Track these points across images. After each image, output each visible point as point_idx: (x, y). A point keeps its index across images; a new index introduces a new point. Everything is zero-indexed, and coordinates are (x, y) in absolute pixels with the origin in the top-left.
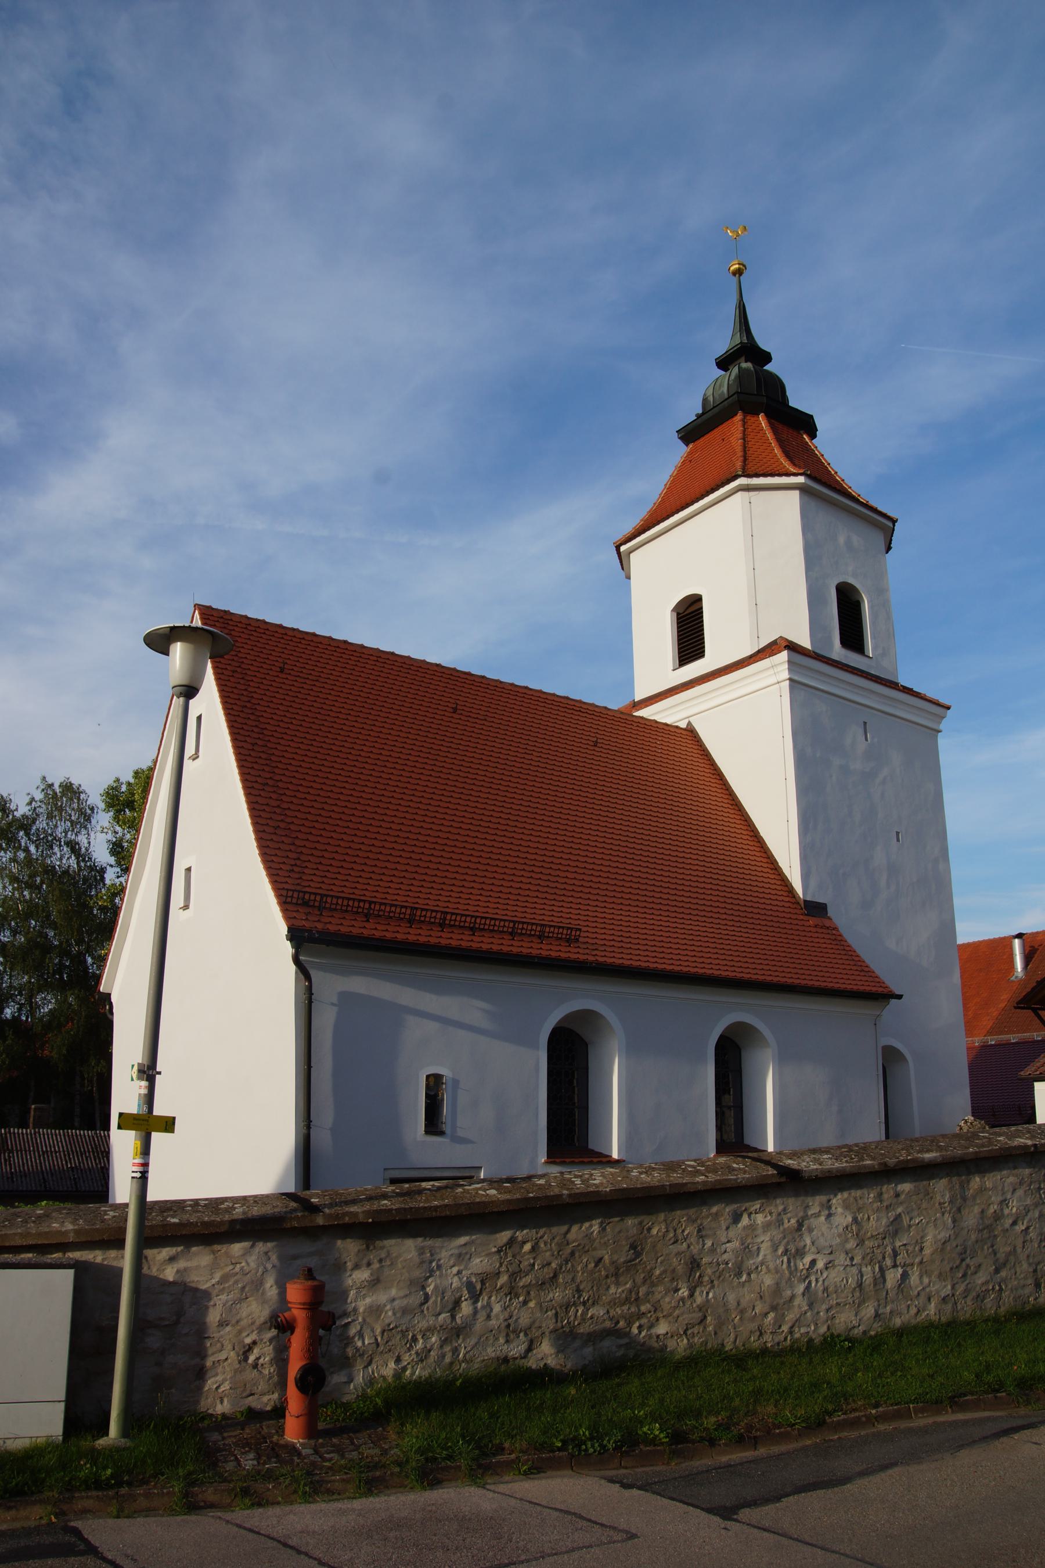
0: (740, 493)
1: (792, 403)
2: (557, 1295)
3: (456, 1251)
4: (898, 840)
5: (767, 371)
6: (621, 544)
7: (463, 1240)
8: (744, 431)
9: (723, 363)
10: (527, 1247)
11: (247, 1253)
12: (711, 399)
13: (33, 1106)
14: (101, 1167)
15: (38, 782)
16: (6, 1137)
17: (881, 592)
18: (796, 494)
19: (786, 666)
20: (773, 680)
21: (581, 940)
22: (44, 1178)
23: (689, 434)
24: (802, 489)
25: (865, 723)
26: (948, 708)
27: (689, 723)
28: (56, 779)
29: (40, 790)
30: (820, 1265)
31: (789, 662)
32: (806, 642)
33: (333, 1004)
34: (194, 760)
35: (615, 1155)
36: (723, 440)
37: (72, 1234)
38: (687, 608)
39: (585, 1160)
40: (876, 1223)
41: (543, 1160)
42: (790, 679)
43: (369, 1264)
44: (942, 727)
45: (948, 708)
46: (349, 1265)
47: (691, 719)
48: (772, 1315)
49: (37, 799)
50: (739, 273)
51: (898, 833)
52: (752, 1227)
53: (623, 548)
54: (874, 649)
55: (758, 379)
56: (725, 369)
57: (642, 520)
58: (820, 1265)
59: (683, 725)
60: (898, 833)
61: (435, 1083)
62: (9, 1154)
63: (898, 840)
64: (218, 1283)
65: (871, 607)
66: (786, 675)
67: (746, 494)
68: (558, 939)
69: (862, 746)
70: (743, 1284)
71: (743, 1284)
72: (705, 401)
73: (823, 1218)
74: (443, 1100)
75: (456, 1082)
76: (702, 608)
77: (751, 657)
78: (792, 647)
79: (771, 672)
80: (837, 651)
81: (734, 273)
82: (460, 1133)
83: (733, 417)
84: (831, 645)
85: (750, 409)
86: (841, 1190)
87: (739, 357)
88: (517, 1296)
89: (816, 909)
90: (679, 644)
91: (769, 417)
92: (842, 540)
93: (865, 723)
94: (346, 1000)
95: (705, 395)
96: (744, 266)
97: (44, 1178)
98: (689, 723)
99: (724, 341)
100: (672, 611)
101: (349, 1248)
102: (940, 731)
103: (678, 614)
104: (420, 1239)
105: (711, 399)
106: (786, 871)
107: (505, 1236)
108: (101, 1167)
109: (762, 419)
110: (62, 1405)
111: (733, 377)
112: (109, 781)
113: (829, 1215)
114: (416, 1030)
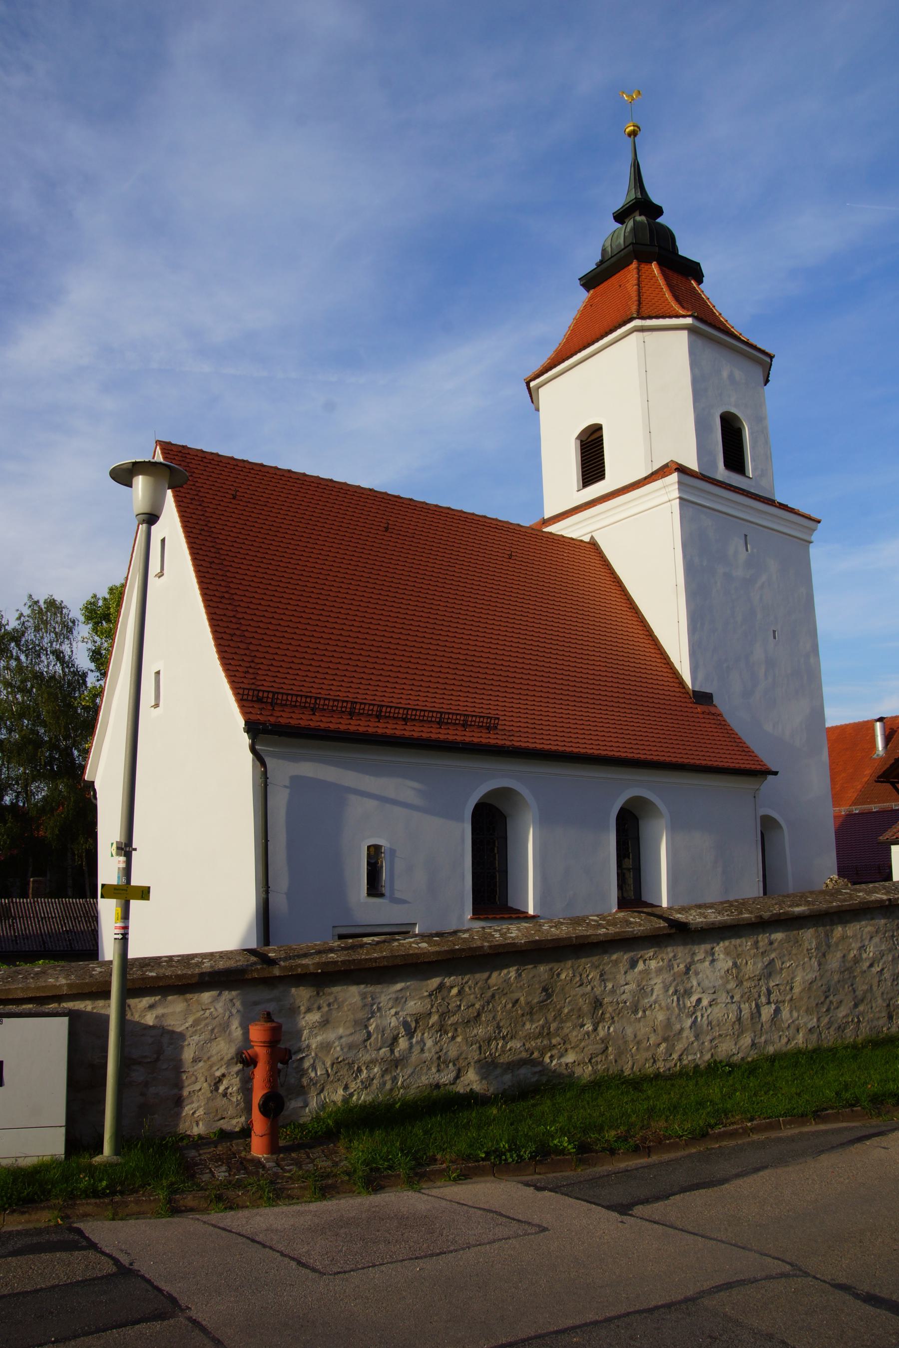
0: (635, 333)
1: (680, 253)
2: (480, 1031)
3: (394, 996)
4: (775, 638)
5: (659, 224)
6: (531, 380)
7: (399, 986)
8: (639, 278)
9: (620, 217)
10: (455, 991)
11: (215, 1000)
12: (609, 249)
13: (32, 879)
14: (92, 930)
15: (26, 600)
16: (10, 907)
17: (759, 419)
18: (684, 334)
19: (676, 486)
20: (666, 499)
21: (499, 727)
22: (43, 940)
23: (590, 282)
24: (690, 329)
25: (746, 536)
26: (819, 522)
27: (592, 537)
28: (41, 598)
29: (27, 607)
30: (705, 1002)
31: (680, 483)
32: (693, 465)
33: (285, 787)
34: (159, 577)
35: (531, 912)
36: (620, 286)
37: (65, 988)
38: (589, 437)
39: (506, 916)
40: (753, 967)
41: (469, 917)
42: (680, 498)
43: (319, 1008)
44: (813, 538)
45: (819, 522)
46: (303, 1009)
47: (594, 534)
48: (664, 1045)
49: (25, 614)
50: (633, 134)
51: (774, 632)
52: (646, 972)
53: (532, 384)
54: (754, 470)
55: (651, 231)
56: (622, 222)
57: (549, 359)
58: (705, 1002)
59: (587, 539)
60: (774, 632)
61: (375, 852)
62: (12, 920)
63: (775, 638)
64: (191, 1026)
65: (751, 434)
66: (676, 494)
67: (640, 334)
68: (479, 727)
69: (743, 556)
70: (639, 1020)
71: (639, 1020)
72: (604, 251)
73: (707, 963)
74: (382, 867)
75: (393, 852)
76: (602, 436)
77: (646, 478)
78: (682, 470)
79: (663, 491)
80: (721, 472)
81: (629, 135)
82: (397, 895)
83: (629, 265)
84: (715, 466)
85: (644, 258)
86: (723, 939)
87: (634, 211)
88: (446, 1033)
89: (703, 698)
90: (582, 468)
91: (661, 265)
92: (725, 374)
93: (746, 536)
94: (298, 784)
95: (604, 246)
96: (639, 128)
97: (43, 940)
98: (592, 537)
99: (621, 197)
100: (577, 438)
101: (302, 995)
102: (811, 542)
103: (581, 441)
104: (362, 986)
105: (609, 249)
106: (677, 666)
107: (435, 982)
108: (92, 930)
109: (654, 266)
110: (63, 1130)
111: (628, 229)
112: (88, 597)
113: (713, 961)
114: (357, 808)
